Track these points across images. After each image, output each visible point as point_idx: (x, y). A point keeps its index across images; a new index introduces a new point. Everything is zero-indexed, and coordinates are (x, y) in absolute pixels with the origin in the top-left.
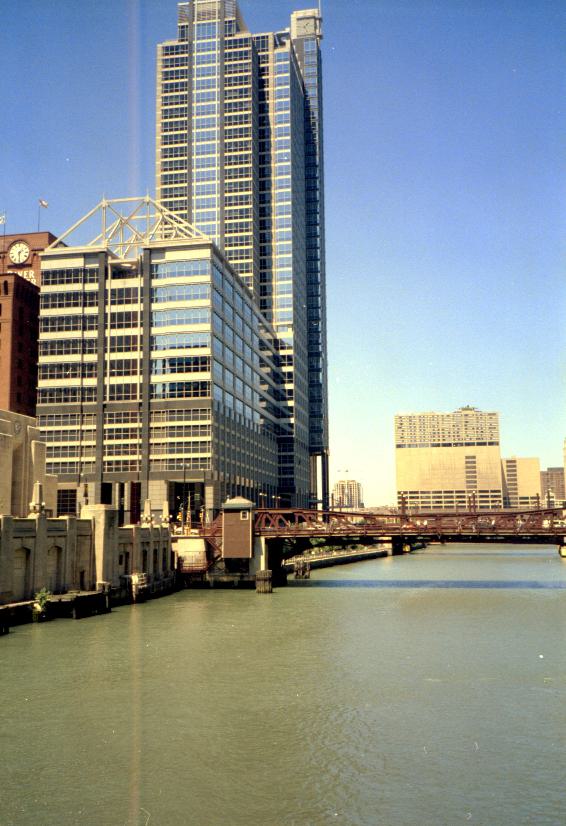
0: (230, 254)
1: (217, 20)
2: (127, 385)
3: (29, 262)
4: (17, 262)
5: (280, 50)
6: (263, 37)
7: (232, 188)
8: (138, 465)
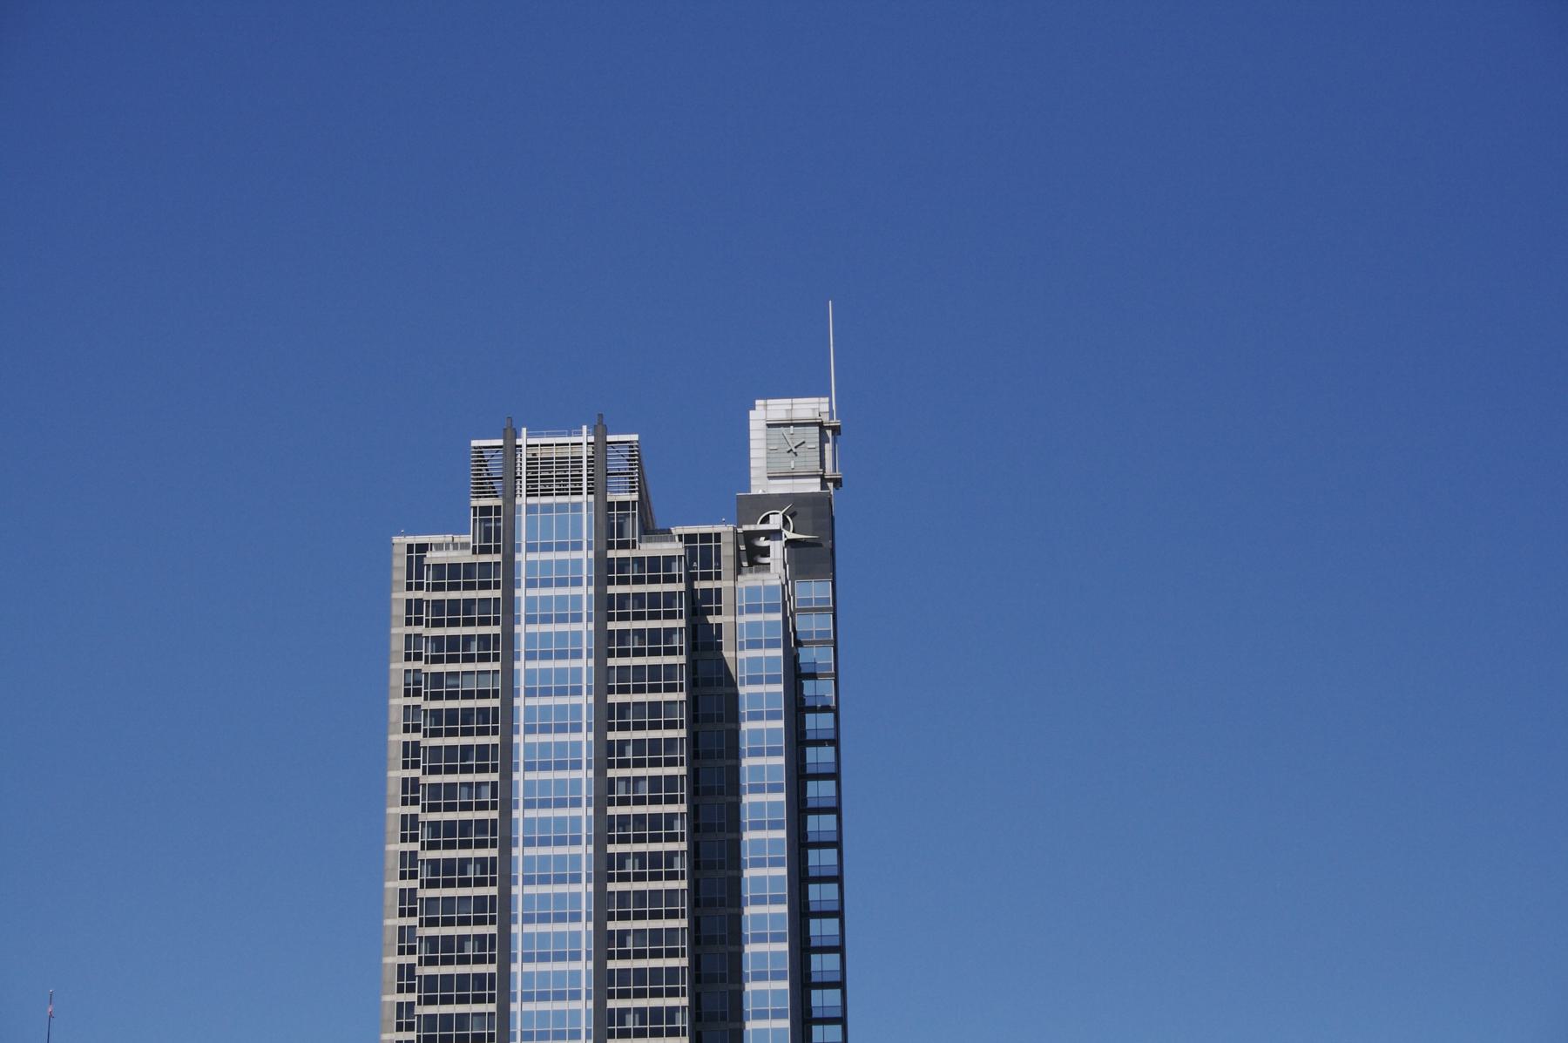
1: (584, 499)
5: (749, 580)
6: (706, 537)
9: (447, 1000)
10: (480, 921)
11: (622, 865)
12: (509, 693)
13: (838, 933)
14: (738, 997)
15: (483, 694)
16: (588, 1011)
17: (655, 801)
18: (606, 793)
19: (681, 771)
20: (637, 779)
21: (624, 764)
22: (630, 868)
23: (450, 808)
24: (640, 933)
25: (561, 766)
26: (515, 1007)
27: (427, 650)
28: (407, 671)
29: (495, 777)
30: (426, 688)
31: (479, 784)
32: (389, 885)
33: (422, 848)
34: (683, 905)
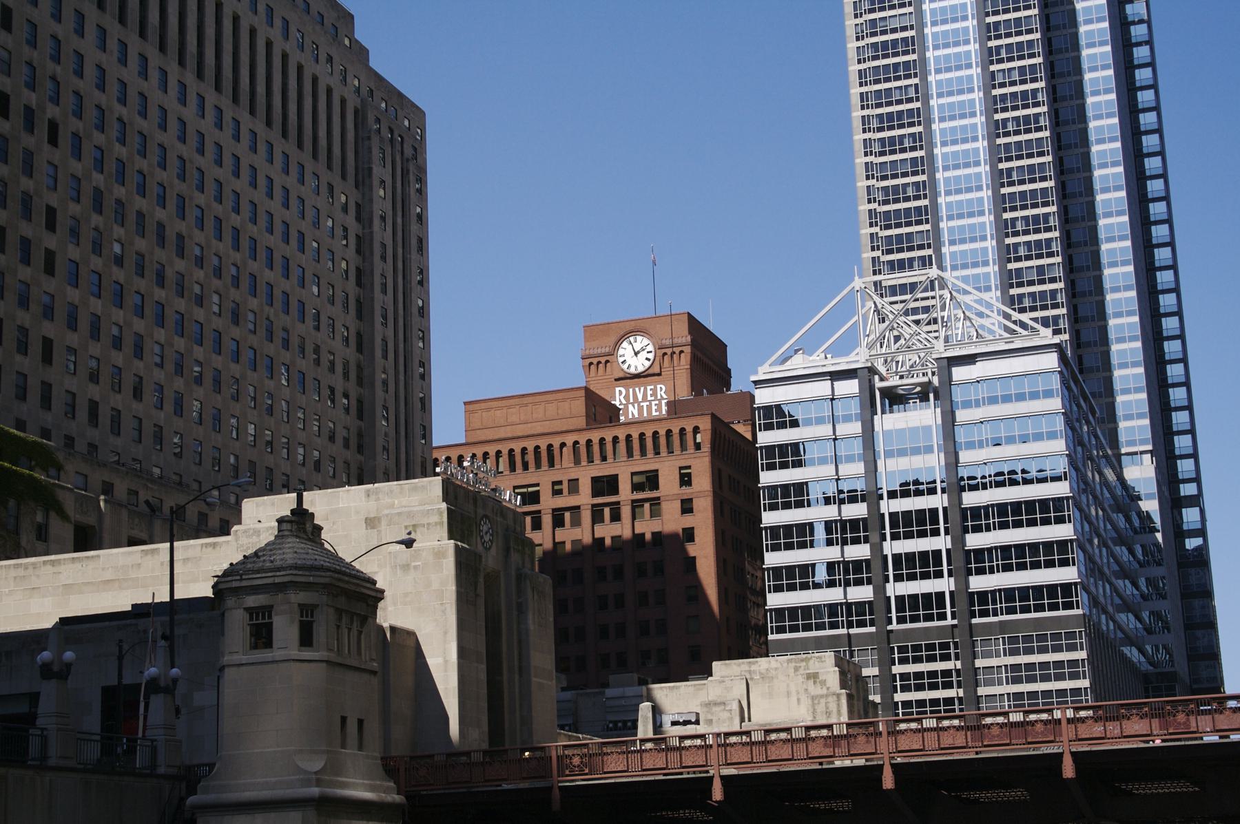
0: (895, 71)
2: (921, 513)
3: (656, 369)
4: (632, 370)
7: (1009, 153)
8: (954, 679)
9: (898, 225)
10: (915, 173)
11: (1005, 126)
12: (921, 25)
13: (1166, 211)
14: (1092, 205)
15: (904, 29)
16: (990, 222)
17: (1023, 82)
18: (990, 81)
19: (1051, 184)
20: (1010, 70)
21: (1000, 61)
22: (1019, 227)
23: (889, 104)
24: (1021, 168)
25: (959, 68)
26: (943, 225)
27: (876, 148)
28: (856, 25)
29: (916, 81)
30: (877, 173)
31: (906, 87)
32: (858, 161)
33: (883, 254)
34: (1050, 172)
